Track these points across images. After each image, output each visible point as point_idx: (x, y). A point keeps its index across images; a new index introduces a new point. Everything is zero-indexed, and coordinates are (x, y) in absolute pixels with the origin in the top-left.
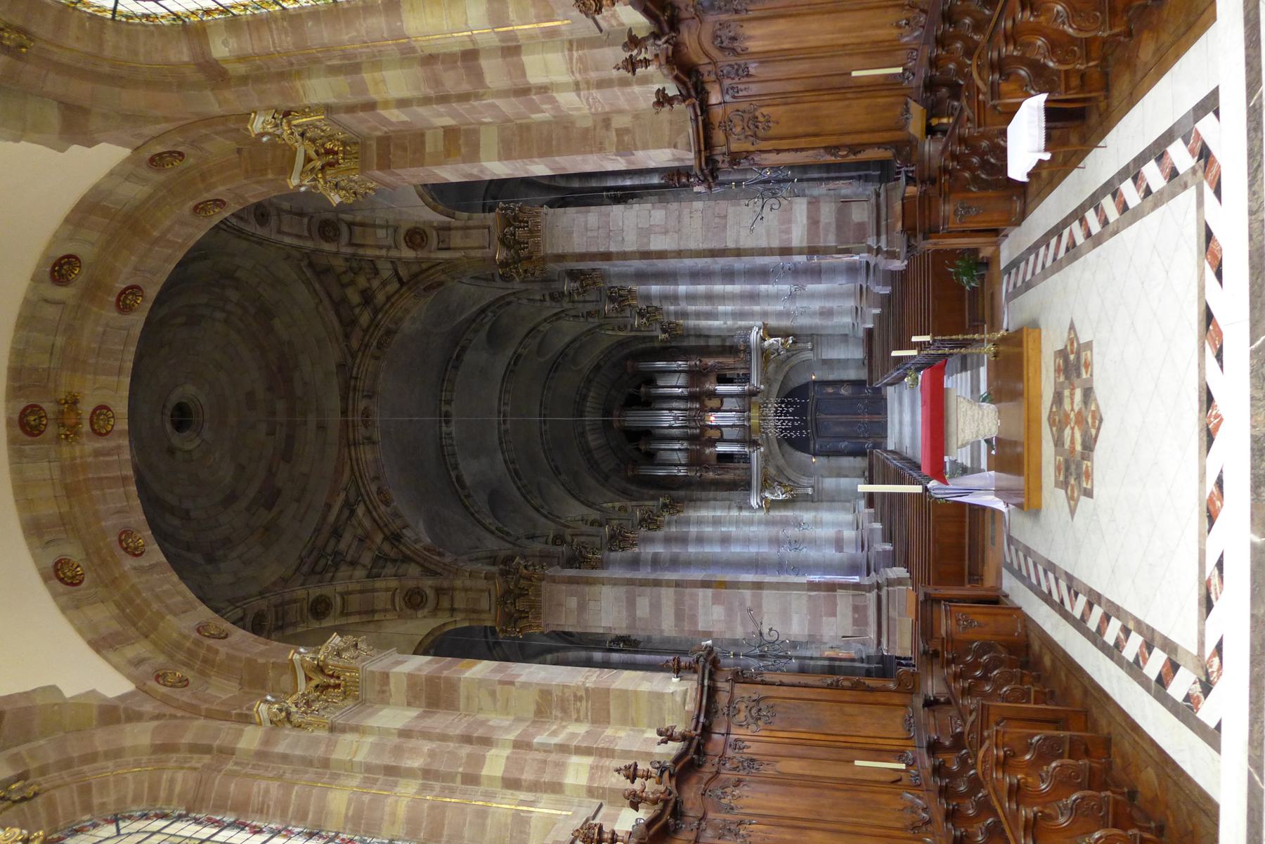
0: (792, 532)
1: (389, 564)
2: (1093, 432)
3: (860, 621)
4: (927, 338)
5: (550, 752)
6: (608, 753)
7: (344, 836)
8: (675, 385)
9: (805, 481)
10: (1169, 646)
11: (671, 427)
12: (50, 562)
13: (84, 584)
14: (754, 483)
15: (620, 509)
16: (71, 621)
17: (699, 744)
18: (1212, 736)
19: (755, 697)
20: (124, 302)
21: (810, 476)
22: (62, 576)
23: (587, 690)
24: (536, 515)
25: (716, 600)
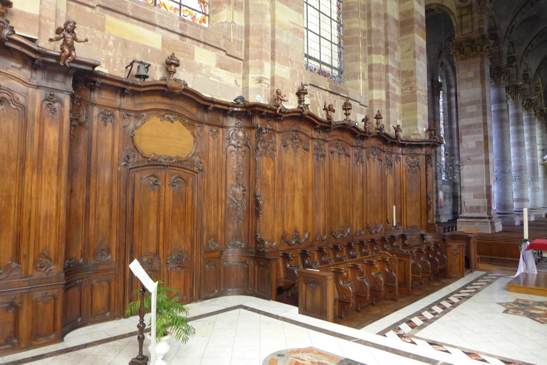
0: (527, 176)
2: (538, 319)
3: (472, 209)
5: (386, 81)
6: (388, 105)
7: (341, 5)
10: (422, 327)
15: (538, 87)
17: (396, 143)
18: (383, 333)
19: (420, 164)
23: (415, 91)
25: (478, 143)
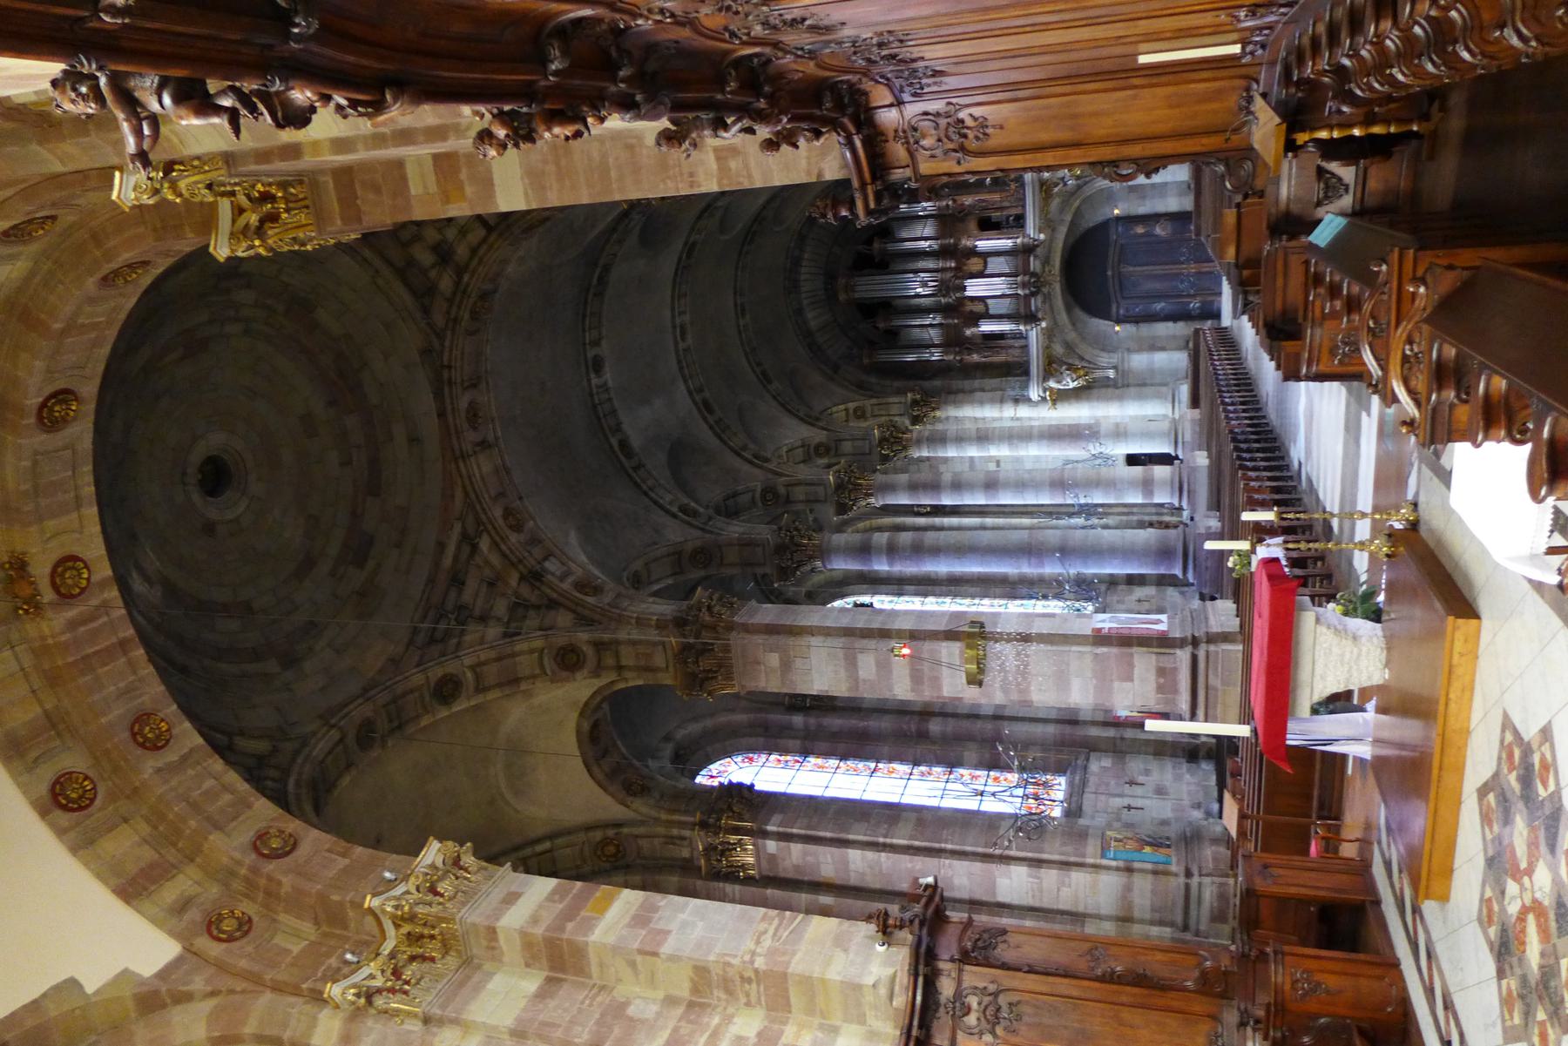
1: (532, 613)
4: (1267, 516)
8: (922, 236)
9: (1104, 359)
11: (918, 296)
12: (43, 789)
13: (97, 802)
14: (1034, 369)
15: (855, 410)
16: (86, 864)
19: (992, 988)
20: (52, 412)
21: (1113, 350)
22: (65, 801)
23: (756, 971)
24: (737, 463)
